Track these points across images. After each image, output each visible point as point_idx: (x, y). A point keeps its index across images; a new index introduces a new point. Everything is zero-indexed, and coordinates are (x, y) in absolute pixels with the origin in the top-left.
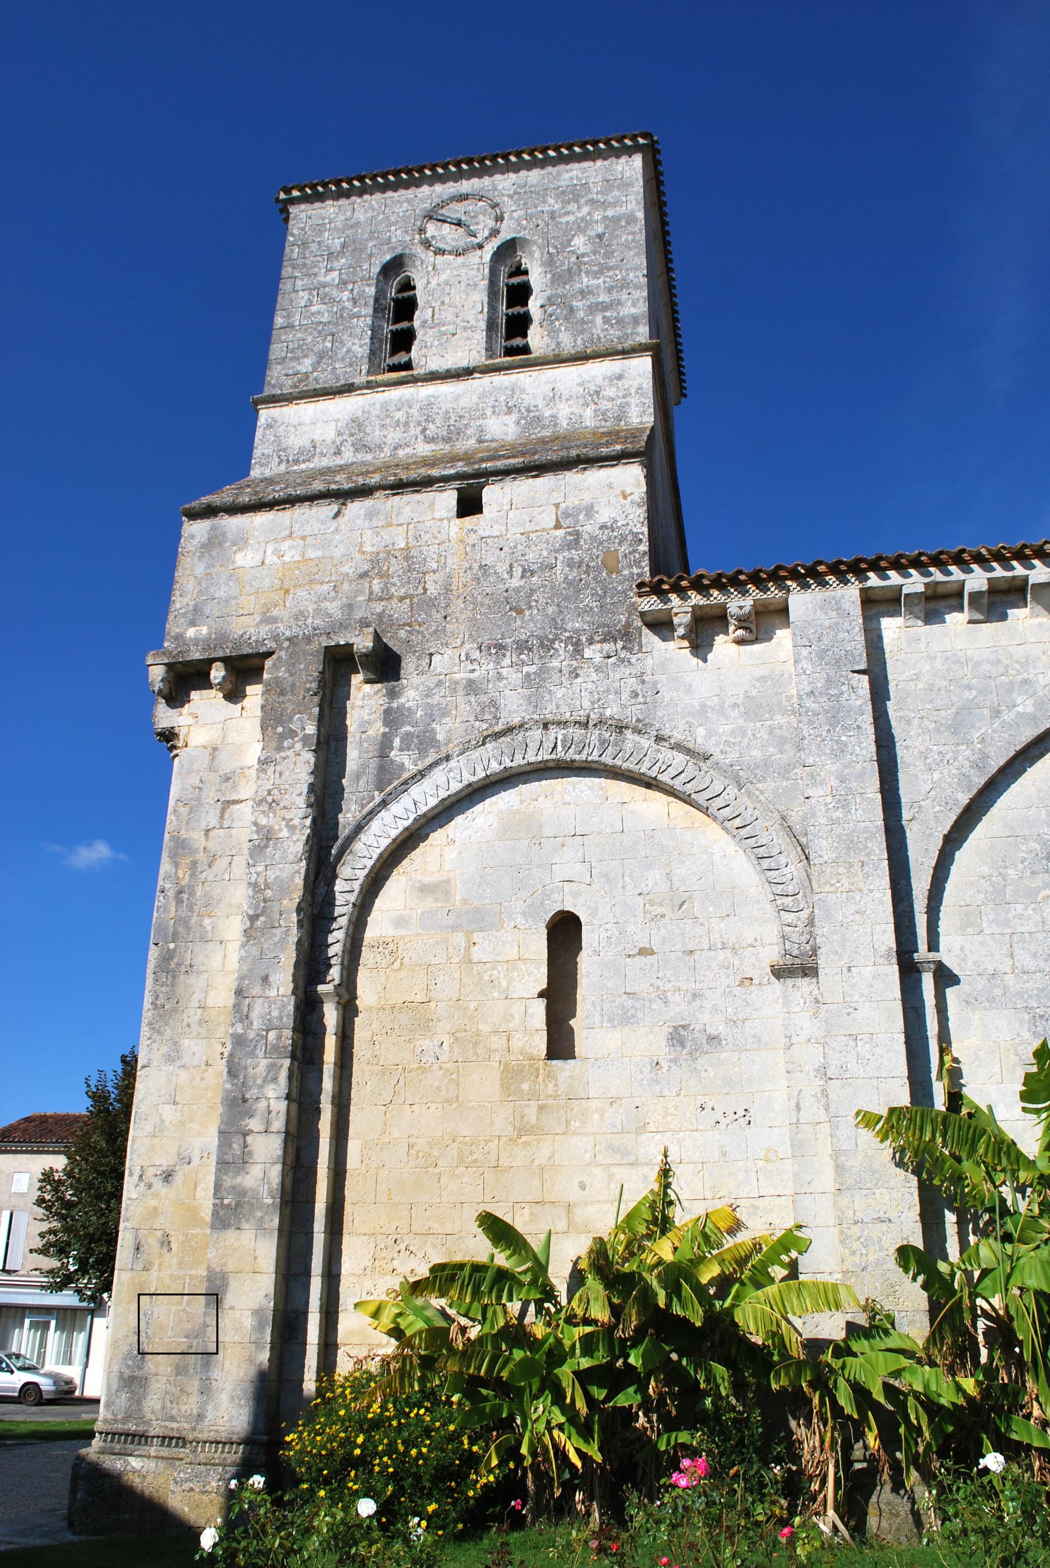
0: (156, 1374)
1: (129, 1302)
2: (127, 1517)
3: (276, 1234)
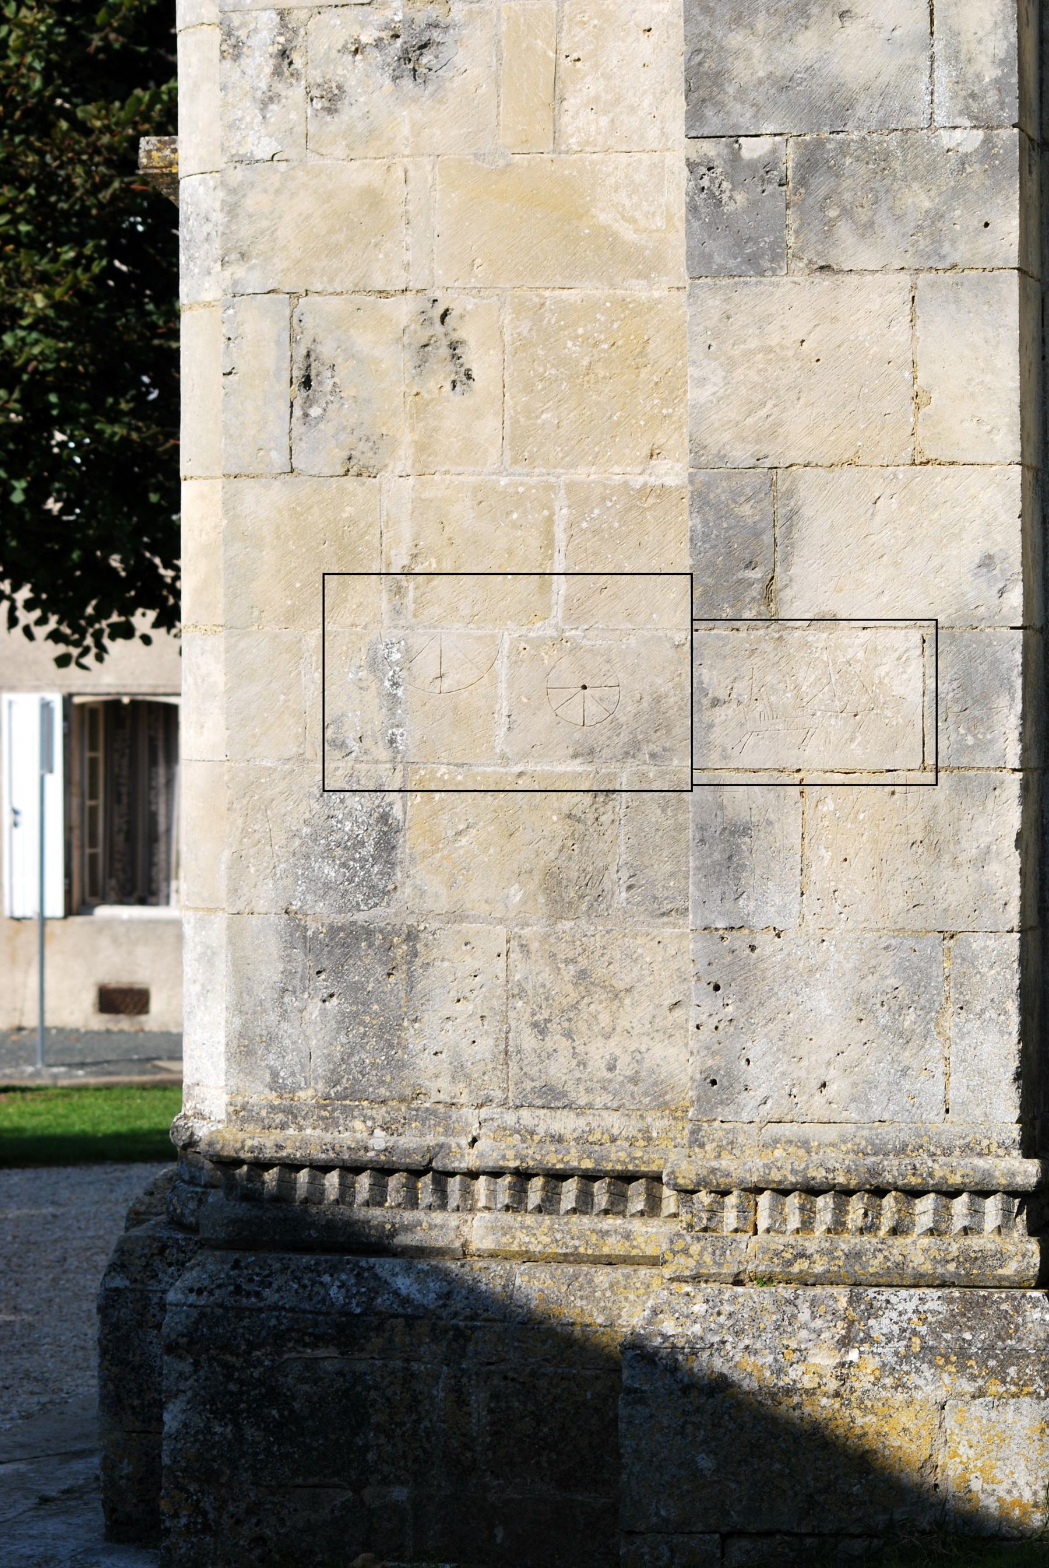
0: (456, 916)
1: (291, 617)
2: (400, 1494)
3: (1010, 286)
